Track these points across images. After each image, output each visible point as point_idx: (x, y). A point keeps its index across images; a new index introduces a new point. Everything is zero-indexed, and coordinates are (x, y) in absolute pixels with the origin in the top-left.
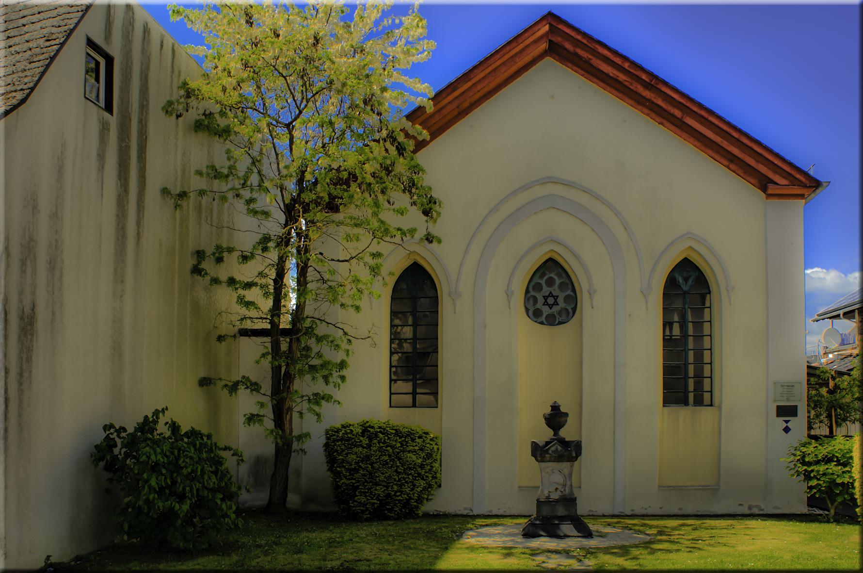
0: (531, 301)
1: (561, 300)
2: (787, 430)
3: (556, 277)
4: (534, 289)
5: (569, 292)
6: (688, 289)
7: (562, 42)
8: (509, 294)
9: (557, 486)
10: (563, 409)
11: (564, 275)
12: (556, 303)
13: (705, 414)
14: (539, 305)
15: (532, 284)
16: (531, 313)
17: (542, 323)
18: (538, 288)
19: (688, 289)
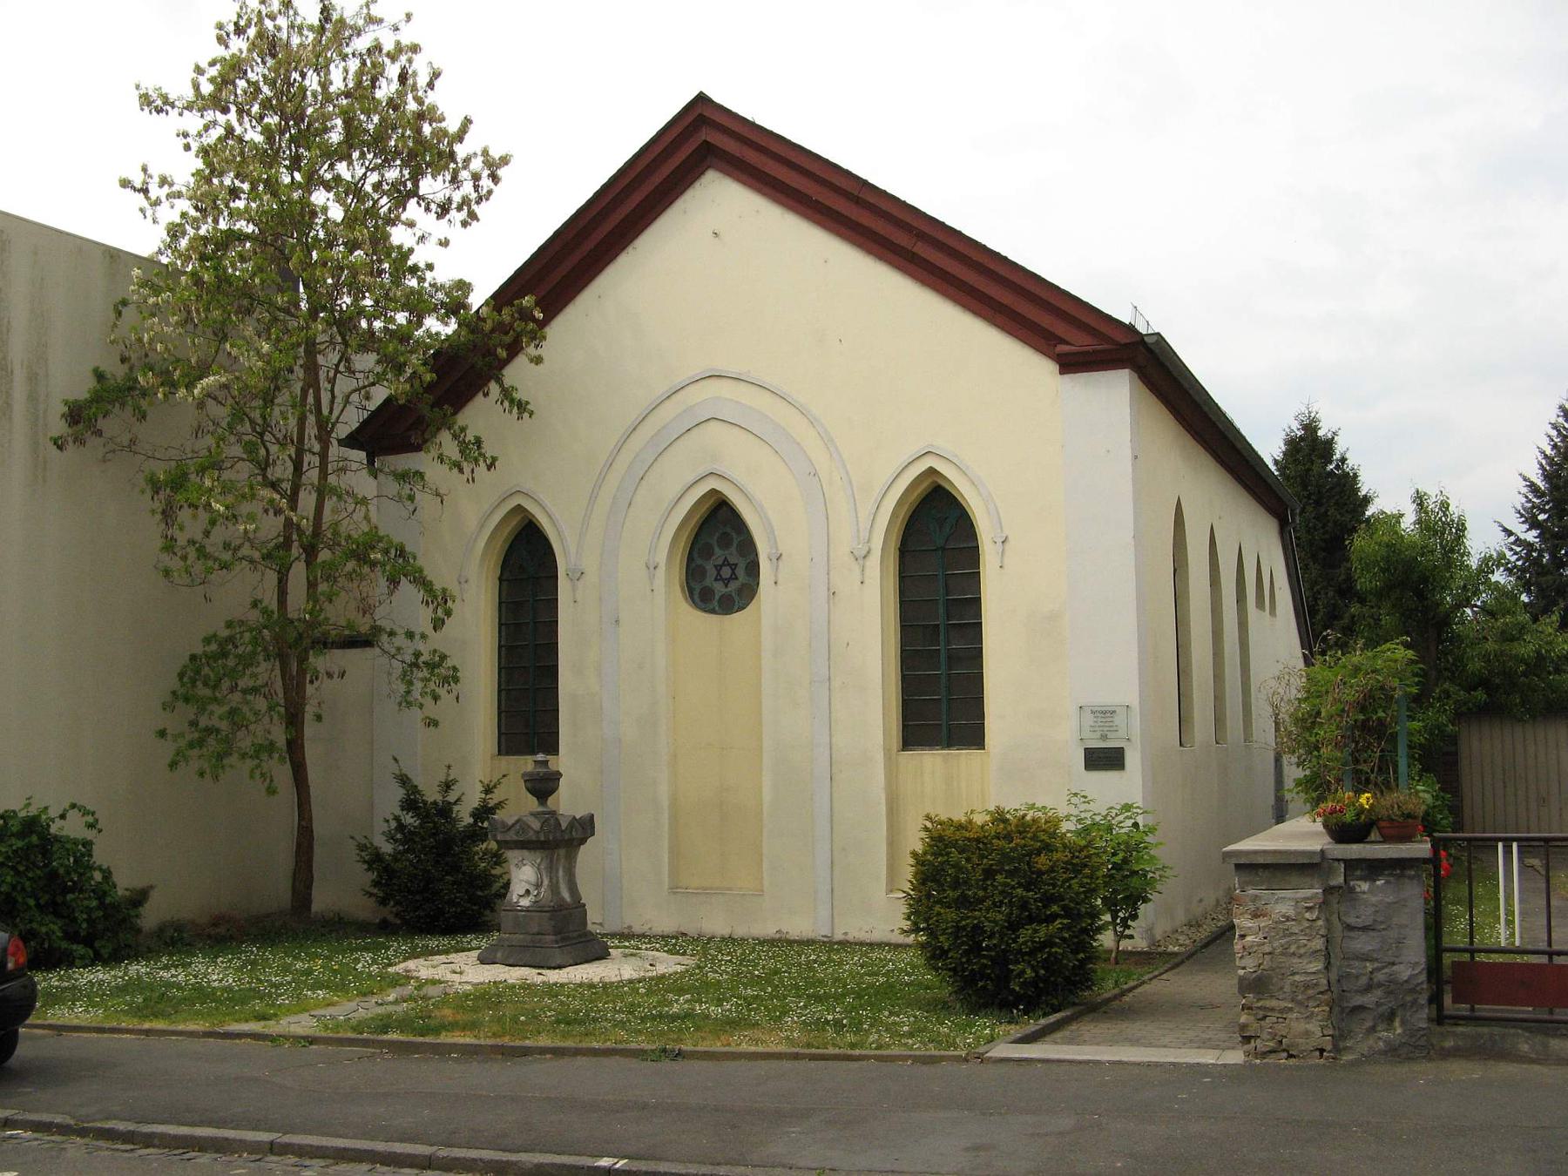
1: (712, 573)
6: (935, 542)
7: (702, 143)
12: (734, 577)
13: (965, 758)
14: (709, 581)
16: (696, 593)
17: (713, 611)
18: (707, 552)
19: (935, 542)
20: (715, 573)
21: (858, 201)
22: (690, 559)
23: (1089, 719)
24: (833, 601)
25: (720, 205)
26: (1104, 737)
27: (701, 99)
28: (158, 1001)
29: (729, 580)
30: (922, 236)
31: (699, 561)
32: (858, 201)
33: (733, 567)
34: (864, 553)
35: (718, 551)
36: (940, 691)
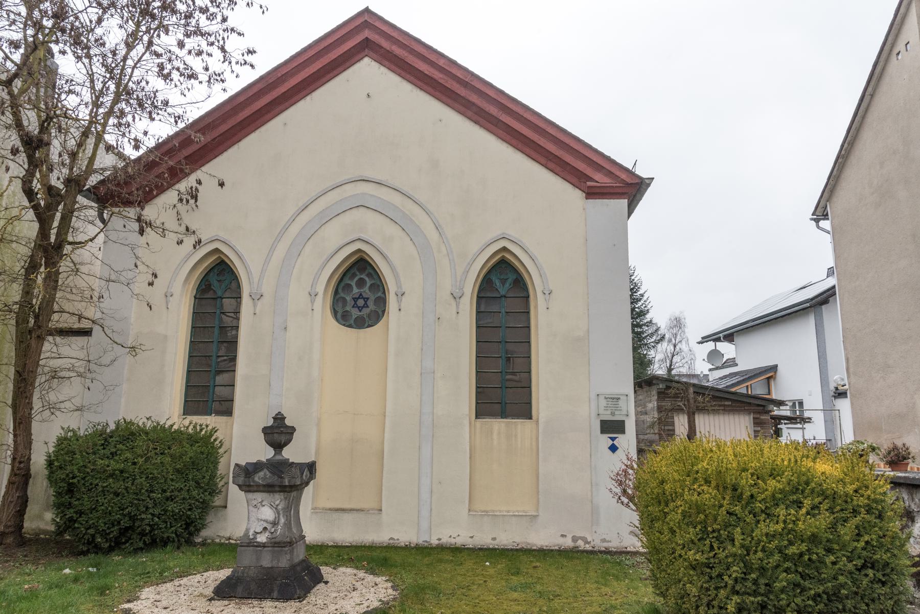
0: (340, 304)
2: (613, 448)
3: (367, 279)
5: (380, 294)
6: (503, 290)
7: (365, 40)
8: (313, 295)
9: (265, 525)
10: (288, 422)
11: (375, 277)
13: (521, 426)
15: (342, 284)
16: (339, 315)
17: (350, 326)
19: (503, 290)
21: (412, 51)
22: (336, 292)
23: (603, 403)
24: (433, 325)
25: (367, 71)
26: (613, 414)
27: (367, 10)
28: (457, 297)
29: (363, 307)
30: (441, 69)
31: (342, 295)
33: (366, 300)
35: (356, 290)
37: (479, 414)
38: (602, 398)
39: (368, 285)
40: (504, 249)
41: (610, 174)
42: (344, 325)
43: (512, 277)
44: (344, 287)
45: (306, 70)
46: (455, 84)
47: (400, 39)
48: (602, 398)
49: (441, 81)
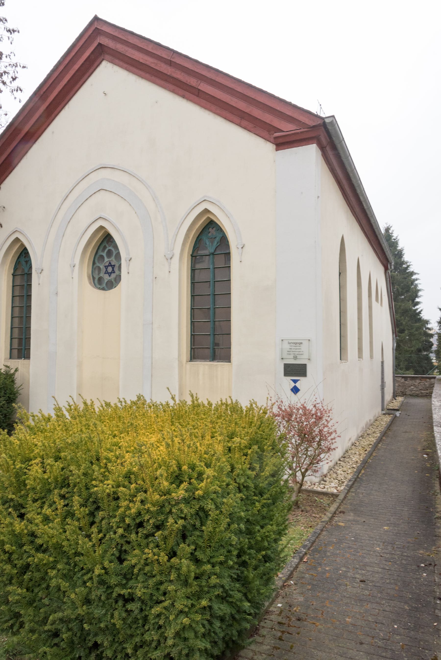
0: (97, 272)
3: (113, 250)
4: (98, 260)
6: (209, 246)
12: (113, 272)
13: (219, 367)
17: (103, 289)
19: (209, 246)
20: (105, 270)
22: (94, 263)
23: (287, 346)
25: (108, 75)
26: (295, 358)
27: (96, 19)
32: (170, 63)
34: (170, 256)
35: (106, 260)
36: (210, 336)
37: (194, 356)
38: (286, 342)
39: (114, 254)
40: (206, 211)
41: (291, 119)
42: (99, 289)
43: (219, 236)
44: (98, 258)
45: (60, 84)
46: (163, 65)
47: (120, 36)
48: (286, 342)
49: (153, 66)
